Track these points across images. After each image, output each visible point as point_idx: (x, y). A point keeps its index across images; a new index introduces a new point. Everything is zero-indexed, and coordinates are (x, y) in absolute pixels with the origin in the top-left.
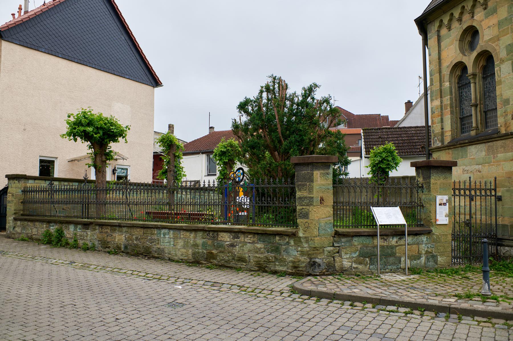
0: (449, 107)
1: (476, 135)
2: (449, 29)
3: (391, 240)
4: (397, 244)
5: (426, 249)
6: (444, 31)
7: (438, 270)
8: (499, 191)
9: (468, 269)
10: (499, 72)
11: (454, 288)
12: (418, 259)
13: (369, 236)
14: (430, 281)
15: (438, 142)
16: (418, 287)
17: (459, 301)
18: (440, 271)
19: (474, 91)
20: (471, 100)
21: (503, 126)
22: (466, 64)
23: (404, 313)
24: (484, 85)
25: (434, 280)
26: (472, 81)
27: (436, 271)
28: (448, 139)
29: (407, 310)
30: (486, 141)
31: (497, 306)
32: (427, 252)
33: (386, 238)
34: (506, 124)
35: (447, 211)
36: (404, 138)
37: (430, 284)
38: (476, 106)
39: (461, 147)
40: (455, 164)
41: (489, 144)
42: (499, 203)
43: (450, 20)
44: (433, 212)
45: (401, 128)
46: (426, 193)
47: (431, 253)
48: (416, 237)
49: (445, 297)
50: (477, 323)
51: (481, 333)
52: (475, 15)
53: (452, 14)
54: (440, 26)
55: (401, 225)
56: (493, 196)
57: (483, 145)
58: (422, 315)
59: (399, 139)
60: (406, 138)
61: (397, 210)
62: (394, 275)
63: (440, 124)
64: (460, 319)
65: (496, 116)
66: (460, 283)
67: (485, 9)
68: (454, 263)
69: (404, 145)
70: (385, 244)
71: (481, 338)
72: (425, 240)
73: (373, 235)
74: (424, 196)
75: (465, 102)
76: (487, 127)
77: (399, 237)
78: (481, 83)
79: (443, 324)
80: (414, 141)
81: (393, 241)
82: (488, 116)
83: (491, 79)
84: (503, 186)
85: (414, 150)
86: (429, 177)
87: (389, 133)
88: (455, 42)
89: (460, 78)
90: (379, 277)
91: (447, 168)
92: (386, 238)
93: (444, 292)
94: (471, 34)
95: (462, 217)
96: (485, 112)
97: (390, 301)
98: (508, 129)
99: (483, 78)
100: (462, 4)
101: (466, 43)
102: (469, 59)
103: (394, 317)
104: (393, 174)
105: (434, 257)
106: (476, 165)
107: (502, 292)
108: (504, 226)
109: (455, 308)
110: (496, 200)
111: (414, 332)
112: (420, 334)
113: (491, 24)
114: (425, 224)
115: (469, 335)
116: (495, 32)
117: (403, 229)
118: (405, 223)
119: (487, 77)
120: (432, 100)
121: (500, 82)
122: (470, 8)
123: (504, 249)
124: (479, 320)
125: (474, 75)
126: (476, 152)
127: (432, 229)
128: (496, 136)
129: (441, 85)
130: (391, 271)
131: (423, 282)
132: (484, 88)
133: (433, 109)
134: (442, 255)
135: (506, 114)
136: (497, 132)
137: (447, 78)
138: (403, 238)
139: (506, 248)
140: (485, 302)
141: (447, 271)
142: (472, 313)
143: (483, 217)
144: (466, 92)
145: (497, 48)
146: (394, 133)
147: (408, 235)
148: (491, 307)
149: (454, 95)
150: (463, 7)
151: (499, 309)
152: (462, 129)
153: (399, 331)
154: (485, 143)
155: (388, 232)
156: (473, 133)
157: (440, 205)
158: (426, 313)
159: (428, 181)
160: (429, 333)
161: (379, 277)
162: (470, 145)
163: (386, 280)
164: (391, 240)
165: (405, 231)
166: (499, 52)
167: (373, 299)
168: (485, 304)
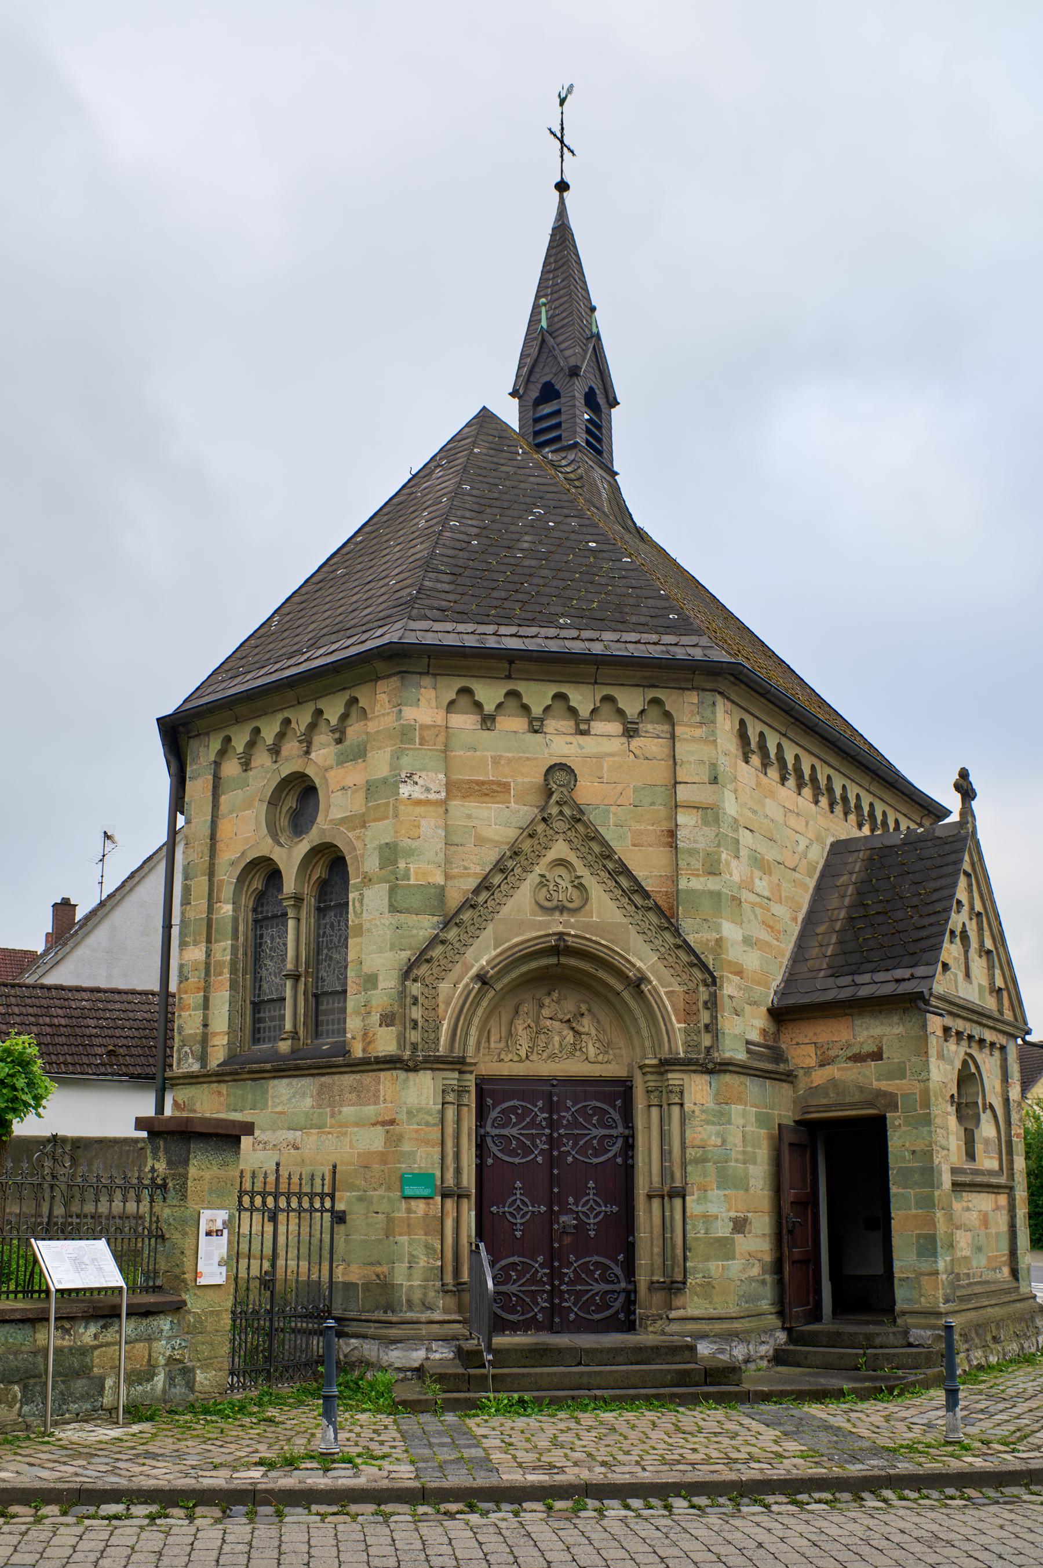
0: (226, 971)
1: (293, 1051)
2: (246, 766)
3: (82, 1330)
4: (96, 1342)
5: (168, 1353)
6: (231, 768)
7: (197, 1405)
8: (341, 1199)
9: (266, 1399)
10: (357, 904)
11: (248, 1446)
12: (148, 1380)
13: (22, 1321)
14: (185, 1436)
15: (191, 1060)
16: (161, 1451)
17: (272, 1474)
18: (203, 1409)
19: (293, 939)
20: (284, 960)
21: (359, 1038)
22: (281, 867)
23: (147, 1517)
24: (318, 926)
25: (195, 1433)
26: (291, 913)
27: (191, 1408)
28: (217, 1056)
29: (154, 1509)
30: (316, 1071)
31: (355, 1476)
32: (171, 1360)
33: (68, 1326)
34: (365, 1034)
35: (224, 1251)
36: (56, 1021)
37: (189, 1443)
38: (296, 978)
39: (254, 1080)
40: (248, 1128)
41: (323, 1079)
42: (340, 1229)
43: (251, 745)
44: (189, 1253)
45: (49, 988)
46: (175, 1202)
47: (180, 1361)
48: (145, 1322)
49: (235, 1469)
50: (318, 1518)
51: (336, 1535)
52: (314, 748)
53: (257, 731)
54: (222, 753)
55: (113, 1289)
56: (327, 1211)
57: (307, 1081)
58: (191, 1518)
59: (41, 1020)
60: (63, 1021)
61: (100, 1248)
62: (88, 1427)
63: (200, 1013)
64: (279, 1514)
65: (343, 1010)
66: (258, 1434)
67: (339, 741)
68: (232, 1385)
69: (57, 1040)
70: (66, 1343)
71: (337, 1546)
72: (167, 1327)
73: (38, 1319)
74: (167, 1211)
75: (268, 962)
76: (317, 1034)
77: (101, 1323)
78: (312, 920)
79: (248, 1528)
80: (87, 1031)
81: (87, 1334)
82: (322, 1008)
83: (335, 916)
84: (352, 1188)
85: (85, 1060)
86: (186, 1162)
87: (13, 1000)
88: (256, 803)
89: (261, 898)
90: (52, 1435)
91: (227, 1137)
92: (68, 1326)
93: (230, 1458)
94: (299, 796)
95: (255, 1264)
96: (316, 996)
97: (105, 1491)
98: (370, 1048)
99: (319, 909)
100: (287, 714)
101: (285, 809)
102: (289, 857)
103: (126, 1533)
104: (25, 1127)
105: (187, 1373)
106: (289, 1129)
107: (357, 1445)
108: (349, 1287)
109: (266, 1491)
110: (332, 1223)
111: (189, 1555)
112: (204, 1559)
113: (349, 781)
114: (166, 1287)
115: (312, 1543)
116: (356, 804)
117: (113, 1300)
118: (121, 1283)
119: (328, 908)
120: (183, 944)
121: (360, 930)
122: (303, 728)
123: (348, 1344)
124: (322, 1512)
125: (298, 899)
126: (290, 1096)
127: (186, 1297)
128: (340, 1060)
129: (210, 909)
130: (78, 1418)
131: (170, 1440)
132: (318, 935)
133: (185, 970)
134: (206, 1366)
135: (366, 1010)
136: (343, 1049)
137: (227, 891)
138: (111, 1324)
139: (353, 1341)
140: (328, 1470)
141: (219, 1407)
142: (305, 1498)
143: (304, 1264)
144: (272, 939)
145: (358, 844)
146: (28, 1001)
147: (129, 1315)
148: (342, 1478)
149: (241, 939)
150: (287, 722)
151: (361, 1482)
152: (256, 1031)
153: (153, 1558)
154: (313, 1075)
155: (75, 1309)
156: (284, 1047)
157: (209, 1234)
158: (199, 1510)
159: (181, 1170)
160: (224, 1551)
161: (52, 1435)
162: (274, 1078)
163: (73, 1443)
164: (82, 1330)
165: (120, 1306)
166: (362, 856)
167: (61, 1491)
168: (329, 1474)
